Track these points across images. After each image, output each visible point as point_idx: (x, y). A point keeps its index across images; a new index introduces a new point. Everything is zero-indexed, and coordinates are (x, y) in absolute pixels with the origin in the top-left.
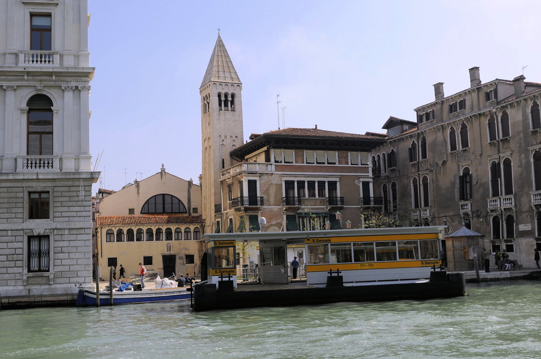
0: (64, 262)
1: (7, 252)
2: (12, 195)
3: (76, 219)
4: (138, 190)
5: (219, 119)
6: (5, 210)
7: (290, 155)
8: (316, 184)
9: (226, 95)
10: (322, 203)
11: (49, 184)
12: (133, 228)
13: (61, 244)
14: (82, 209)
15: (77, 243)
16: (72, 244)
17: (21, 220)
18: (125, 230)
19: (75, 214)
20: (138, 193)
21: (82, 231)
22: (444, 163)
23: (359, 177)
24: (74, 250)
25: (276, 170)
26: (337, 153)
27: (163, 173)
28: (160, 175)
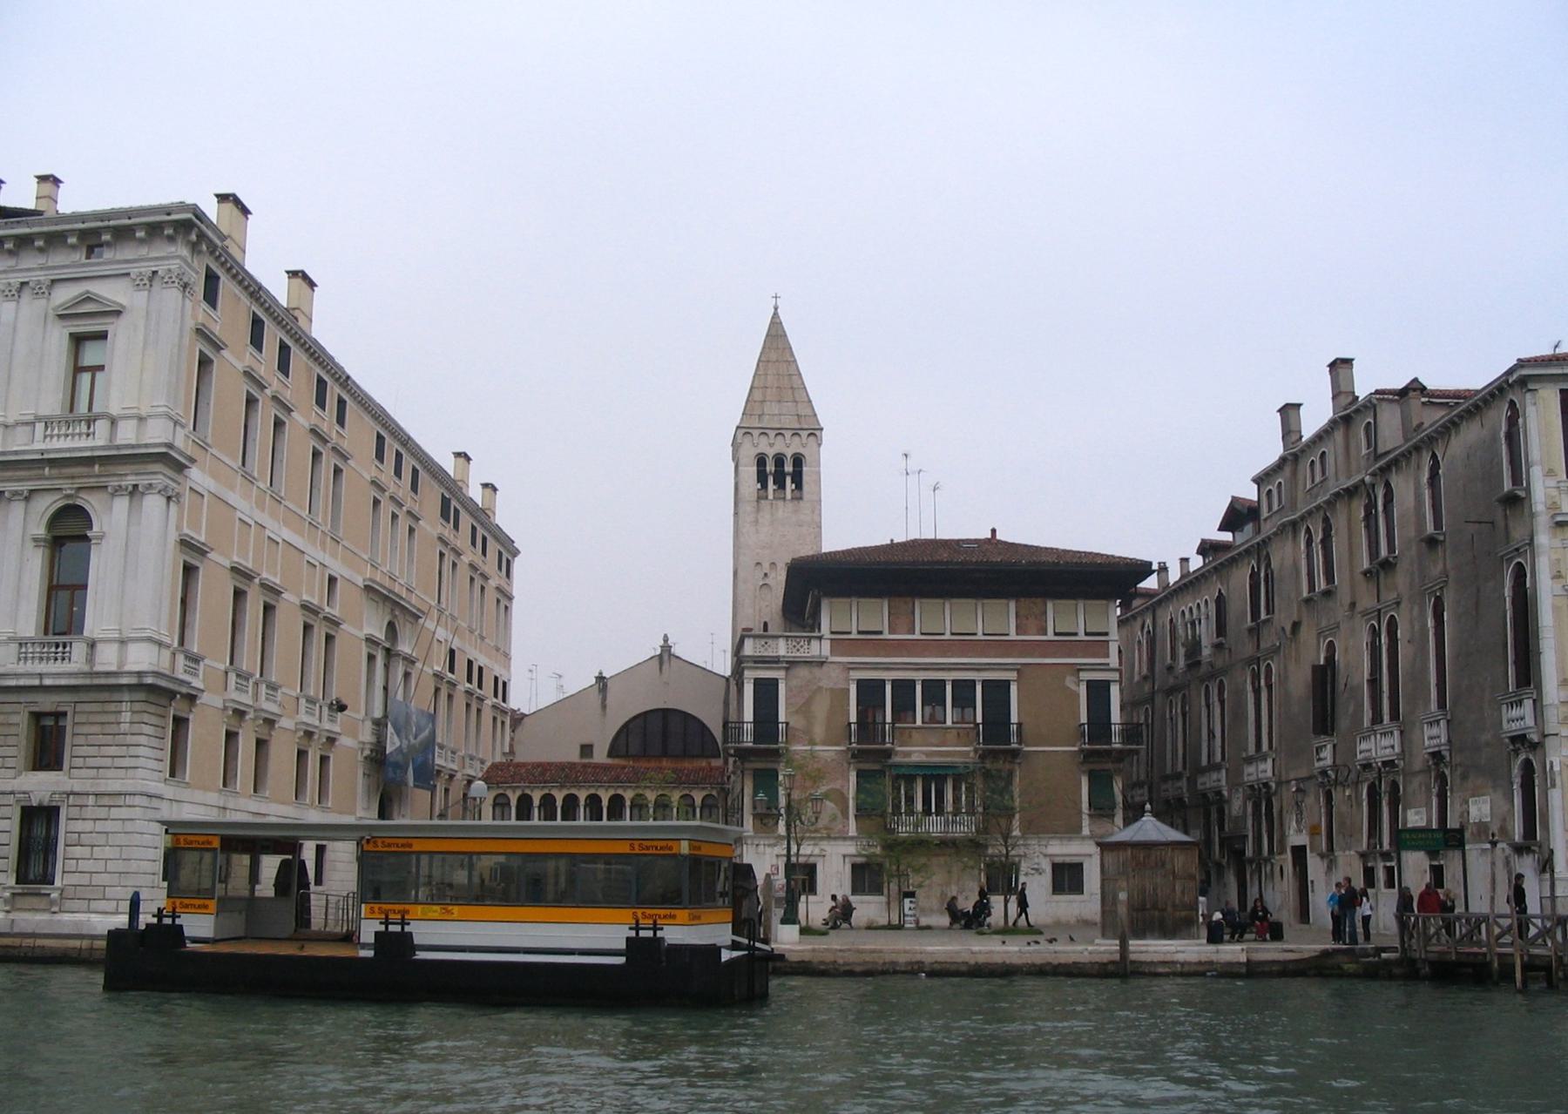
0: (83, 865)
3: (111, 773)
4: (604, 699)
5: (757, 521)
7: (872, 616)
8: (888, 688)
10: (961, 738)
11: (67, 697)
12: (554, 792)
13: (78, 826)
14: (123, 751)
15: (109, 826)
16: (100, 826)
17: (11, 773)
18: (536, 798)
19: (108, 762)
20: (604, 706)
21: (129, 800)
23: (1078, 669)
24: (101, 839)
25: (832, 652)
26: (1012, 605)
27: (666, 655)
28: (656, 662)
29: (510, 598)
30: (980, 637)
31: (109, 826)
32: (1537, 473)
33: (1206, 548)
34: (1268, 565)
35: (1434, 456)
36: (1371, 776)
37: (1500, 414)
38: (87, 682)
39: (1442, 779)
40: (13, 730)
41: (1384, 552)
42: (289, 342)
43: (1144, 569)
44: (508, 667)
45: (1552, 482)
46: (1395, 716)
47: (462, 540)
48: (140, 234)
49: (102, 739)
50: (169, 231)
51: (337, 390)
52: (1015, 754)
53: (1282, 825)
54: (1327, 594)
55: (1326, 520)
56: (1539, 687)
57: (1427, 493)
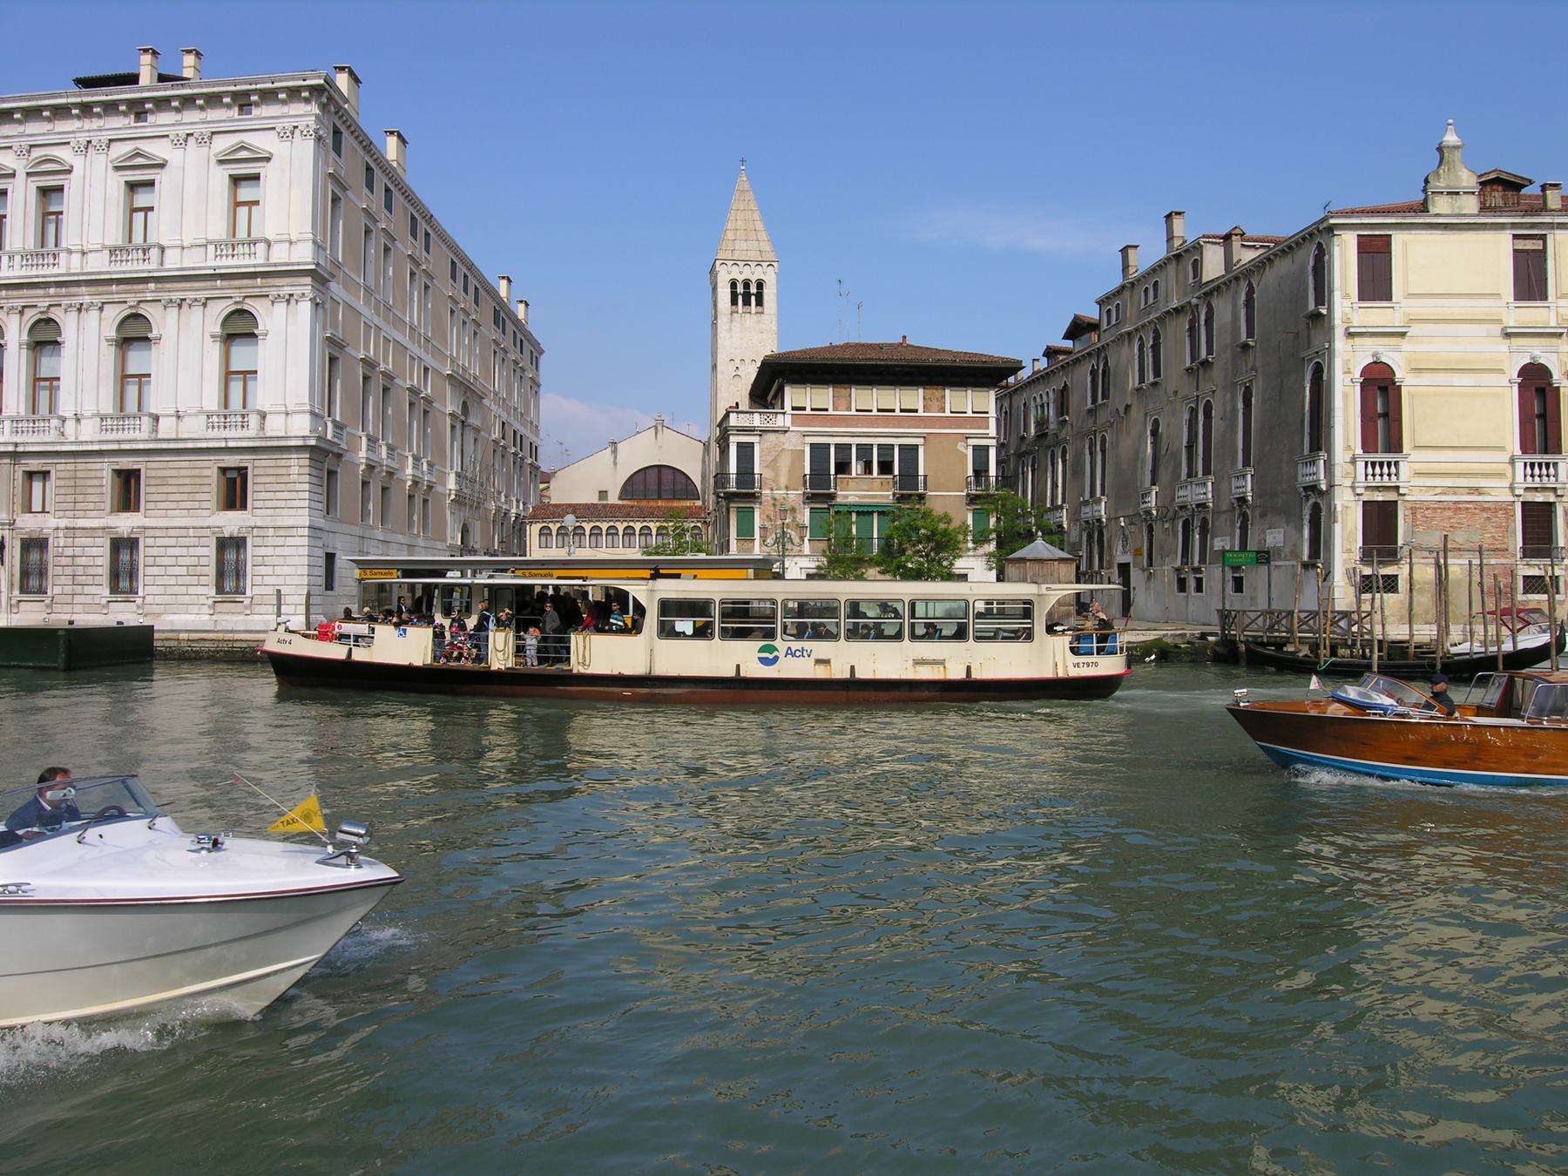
1: (188, 561)
2: (196, 472)
3: (285, 512)
6: (185, 497)
8: (832, 449)
9: (747, 284)
13: (262, 551)
14: (294, 495)
15: (286, 551)
16: (279, 551)
19: (282, 504)
21: (294, 532)
22: (1128, 407)
24: (281, 561)
26: (921, 391)
29: (538, 385)
30: (970, 414)
31: (286, 551)
32: (1337, 295)
33: (1050, 353)
34: (1106, 364)
35: (1250, 285)
36: (1185, 514)
37: (1308, 255)
38: (263, 444)
39: (1244, 516)
40: (206, 481)
41: (1203, 354)
42: (391, 187)
43: (1015, 367)
44: (537, 435)
45: (1347, 303)
46: (1207, 471)
47: (507, 343)
48: (282, 96)
49: (278, 487)
50: (305, 94)
51: (424, 225)
52: (921, 497)
53: (1110, 547)
54: (1155, 384)
55: (1156, 332)
56: (1329, 451)
57: (1243, 312)
